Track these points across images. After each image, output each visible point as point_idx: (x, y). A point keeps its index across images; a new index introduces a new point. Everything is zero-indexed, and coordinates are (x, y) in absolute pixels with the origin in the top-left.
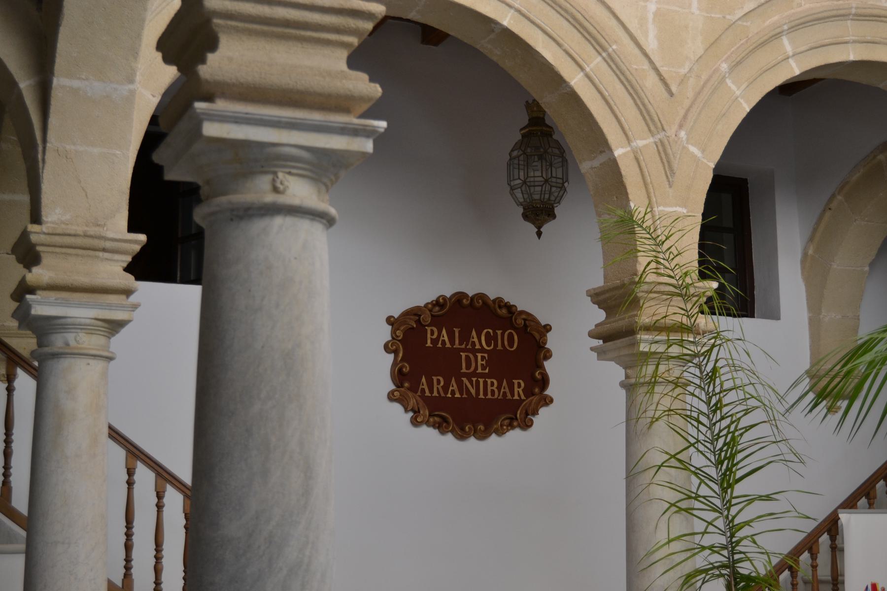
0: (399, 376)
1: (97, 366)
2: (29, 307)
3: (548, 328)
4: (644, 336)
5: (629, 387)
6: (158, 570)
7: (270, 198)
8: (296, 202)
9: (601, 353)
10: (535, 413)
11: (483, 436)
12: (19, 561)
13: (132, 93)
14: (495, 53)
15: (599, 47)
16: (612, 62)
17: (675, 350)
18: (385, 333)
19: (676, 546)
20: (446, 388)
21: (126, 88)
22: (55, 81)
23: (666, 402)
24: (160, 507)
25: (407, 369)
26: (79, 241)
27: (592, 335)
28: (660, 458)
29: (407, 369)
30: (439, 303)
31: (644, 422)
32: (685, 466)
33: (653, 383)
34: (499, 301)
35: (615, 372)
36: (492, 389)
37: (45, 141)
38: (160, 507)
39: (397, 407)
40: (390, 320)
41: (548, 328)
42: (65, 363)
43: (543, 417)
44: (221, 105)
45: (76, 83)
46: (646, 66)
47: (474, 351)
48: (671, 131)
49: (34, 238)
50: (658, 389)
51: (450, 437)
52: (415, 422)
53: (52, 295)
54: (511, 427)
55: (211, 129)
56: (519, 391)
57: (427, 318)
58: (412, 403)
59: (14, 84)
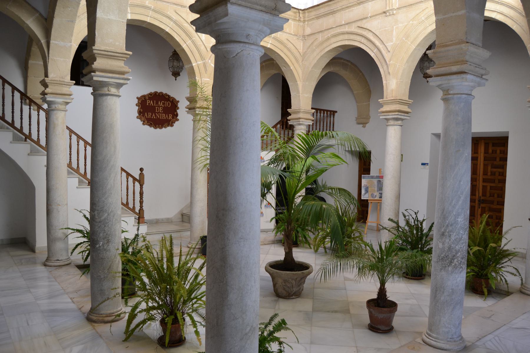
0: (140, 112)
1: (63, 113)
2: (46, 98)
3: (178, 102)
4: (197, 110)
5: (194, 121)
6: (78, 160)
7: (107, 92)
8: (113, 93)
9: (188, 112)
10: (174, 123)
11: (161, 128)
12: (45, 157)
13: (71, 45)
14: (165, 37)
15: (190, 38)
16: (193, 42)
17: (204, 113)
18: (136, 101)
19: (203, 158)
20: (152, 116)
21: (69, 44)
22: (51, 42)
23: (202, 126)
24: (78, 145)
25: (142, 111)
26: (58, 82)
27: (186, 108)
28: (200, 138)
29: (142, 111)
30: (150, 94)
31: (196, 130)
32: (205, 140)
33: (199, 120)
34: (166, 94)
35: (191, 117)
36: (164, 116)
37: (48, 56)
38: (78, 145)
39: (139, 120)
40: (137, 98)
41: (178, 102)
42: (55, 112)
43: (176, 124)
44: (97, 73)
45: (56, 42)
46: (202, 43)
47: (159, 107)
48: (207, 61)
49: (46, 81)
50: (200, 122)
51: (152, 128)
52: (143, 124)
53: (52, 95)
54: (168, 126)
55: (95, 78)
56: (170, 117)
57: (147, 98)
58: (143, 119)
59: (40, 41)
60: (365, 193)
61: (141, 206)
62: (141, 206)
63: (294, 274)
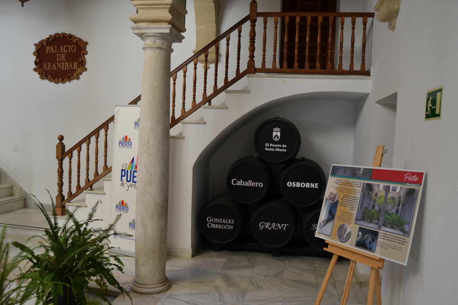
3: (86, 43)
18: (33, 49)
20: (52, 67)
36: (66, 66)
43: (84, 76)
60: (327, 221)
61: (61, 165)
62: (61, 165)
63: (404, 168)
